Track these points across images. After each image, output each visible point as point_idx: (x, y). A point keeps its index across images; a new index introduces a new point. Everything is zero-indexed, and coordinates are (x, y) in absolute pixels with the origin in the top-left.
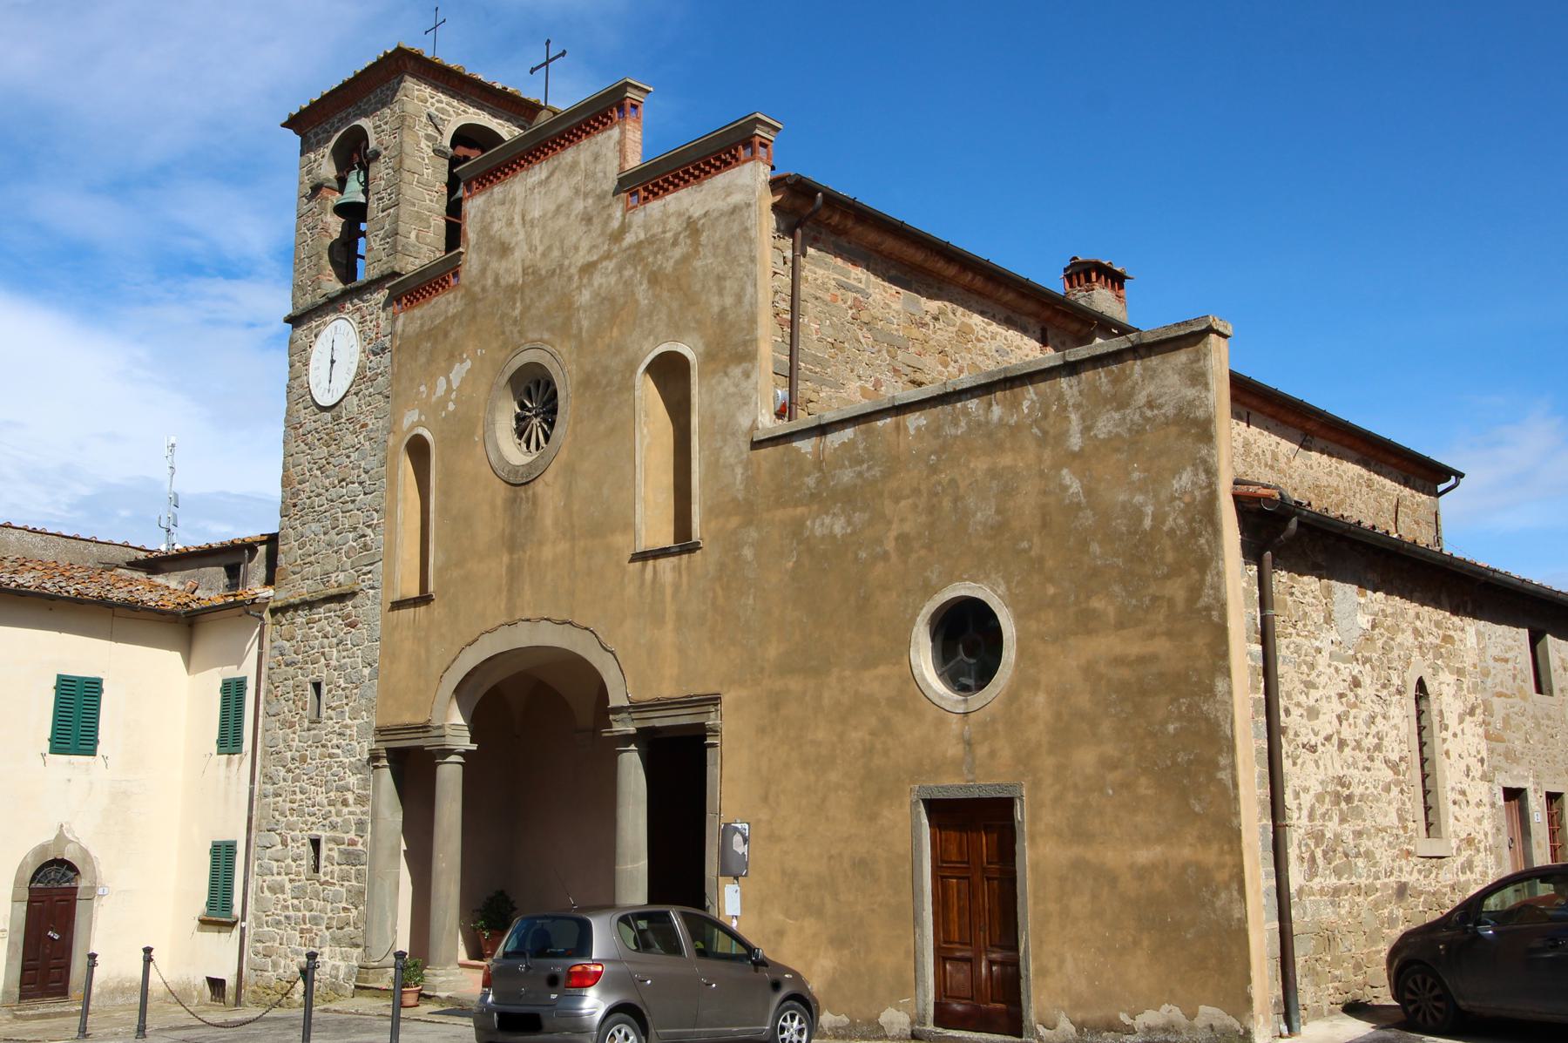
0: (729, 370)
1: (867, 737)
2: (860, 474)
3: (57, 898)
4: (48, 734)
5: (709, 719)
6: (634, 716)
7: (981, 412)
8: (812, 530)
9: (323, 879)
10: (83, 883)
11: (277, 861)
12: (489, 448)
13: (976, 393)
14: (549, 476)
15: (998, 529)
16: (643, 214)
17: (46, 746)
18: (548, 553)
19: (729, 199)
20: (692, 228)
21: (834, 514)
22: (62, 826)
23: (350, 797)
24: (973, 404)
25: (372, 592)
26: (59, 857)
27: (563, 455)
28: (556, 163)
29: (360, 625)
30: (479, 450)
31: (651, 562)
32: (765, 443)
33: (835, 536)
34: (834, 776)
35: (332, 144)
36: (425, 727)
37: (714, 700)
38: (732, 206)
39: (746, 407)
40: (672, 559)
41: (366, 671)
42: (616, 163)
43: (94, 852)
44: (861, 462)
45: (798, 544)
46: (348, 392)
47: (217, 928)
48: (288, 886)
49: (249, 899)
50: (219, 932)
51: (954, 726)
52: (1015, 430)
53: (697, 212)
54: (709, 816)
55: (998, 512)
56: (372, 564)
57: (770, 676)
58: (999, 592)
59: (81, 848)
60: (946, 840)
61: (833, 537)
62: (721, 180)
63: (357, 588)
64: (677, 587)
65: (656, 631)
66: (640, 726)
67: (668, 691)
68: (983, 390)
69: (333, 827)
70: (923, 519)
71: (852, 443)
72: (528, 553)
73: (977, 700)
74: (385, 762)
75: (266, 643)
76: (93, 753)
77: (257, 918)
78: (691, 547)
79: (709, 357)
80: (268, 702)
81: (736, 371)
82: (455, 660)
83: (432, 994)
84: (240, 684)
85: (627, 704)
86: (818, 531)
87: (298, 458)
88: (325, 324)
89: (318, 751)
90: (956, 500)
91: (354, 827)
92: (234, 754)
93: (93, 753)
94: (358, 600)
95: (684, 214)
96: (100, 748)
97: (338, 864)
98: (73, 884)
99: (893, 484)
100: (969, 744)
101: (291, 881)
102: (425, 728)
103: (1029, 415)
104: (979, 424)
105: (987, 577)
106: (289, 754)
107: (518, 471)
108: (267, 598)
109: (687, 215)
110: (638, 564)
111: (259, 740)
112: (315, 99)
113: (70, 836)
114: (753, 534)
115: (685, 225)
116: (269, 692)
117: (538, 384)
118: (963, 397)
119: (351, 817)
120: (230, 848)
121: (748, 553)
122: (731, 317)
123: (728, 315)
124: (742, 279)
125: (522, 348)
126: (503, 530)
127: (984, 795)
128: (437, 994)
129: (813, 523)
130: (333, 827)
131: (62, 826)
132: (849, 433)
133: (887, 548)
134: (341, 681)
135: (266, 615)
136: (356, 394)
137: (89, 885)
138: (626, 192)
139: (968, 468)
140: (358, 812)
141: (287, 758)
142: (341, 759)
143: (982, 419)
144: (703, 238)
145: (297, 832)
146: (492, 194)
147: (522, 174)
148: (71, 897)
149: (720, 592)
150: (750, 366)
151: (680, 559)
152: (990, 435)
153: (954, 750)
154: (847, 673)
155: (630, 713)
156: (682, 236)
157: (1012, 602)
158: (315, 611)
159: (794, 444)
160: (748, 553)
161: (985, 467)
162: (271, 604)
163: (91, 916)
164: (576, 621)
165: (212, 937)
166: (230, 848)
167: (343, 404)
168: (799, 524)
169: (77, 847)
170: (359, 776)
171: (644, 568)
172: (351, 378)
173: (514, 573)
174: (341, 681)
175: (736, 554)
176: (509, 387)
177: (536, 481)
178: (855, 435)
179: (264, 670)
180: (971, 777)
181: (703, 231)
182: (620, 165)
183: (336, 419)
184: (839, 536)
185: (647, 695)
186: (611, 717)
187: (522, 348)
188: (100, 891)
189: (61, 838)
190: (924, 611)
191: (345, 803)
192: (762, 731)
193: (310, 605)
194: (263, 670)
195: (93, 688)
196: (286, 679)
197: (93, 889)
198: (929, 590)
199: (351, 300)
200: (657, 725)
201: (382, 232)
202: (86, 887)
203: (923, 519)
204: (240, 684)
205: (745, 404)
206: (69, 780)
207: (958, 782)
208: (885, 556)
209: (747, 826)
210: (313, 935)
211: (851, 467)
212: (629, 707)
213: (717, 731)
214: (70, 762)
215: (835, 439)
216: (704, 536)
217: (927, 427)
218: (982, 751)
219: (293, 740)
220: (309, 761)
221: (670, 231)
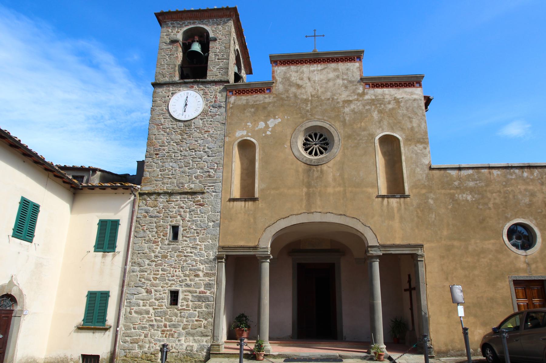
0: (417, 145)
1: (489, 261)
2: (476, 184)
3: (3, 315)
4: (13, 226)
6: (381, 249)
7: (520, 173)
8: (458, 197)
9: (180, 308)
10: (17, 308)
12: (294, 150)
13: (517, 168)
14: (330, 164)
15: (530, 205)
17: (11, 232)
18: (330, 190)
20: (397, 101)
21: (467, 194)
22: (12, 277)
23: (201, 273)
24: (517, 171)
26: (9, 293)
27: (338, 158)
28: (326, 66)
29: (206, 206)
30: (288, 151)
32: (435, 169)
33: (468, 200)
34: (476, 272)
35: (185, 28)
36: (255, 247)
37: (421, 246)
38: (414, 98)
40: (396, 199)
41: (211, 224)
42: (359, 73)
43: (25, 292)
44: (477, 181)
46: (196, 117)
47: (92, 331)
48: (152, 311)
49: (121, 318)
50: (93, 333)
51: (522, 259)
52: (532, 180)
53: (399, 96)
54: (421, 284)
55: (530, 201)
56: (215, 183)
57: (445, 240)
58: (533, 222)
59: (19, 289)
60: (518, 292)
61: (467, 201)
62: (409, 90)
64: (399, 210)
65: (390, 222)
66: (384, 252)
67: (398, 242)
68: (521, 167)
69: (187, 285)
70: (503, 199)
71: (473, 175)
72: (319, 189)
73: (529, 252)
74: (224, 260)
75: (136, 207)
76: (31, 241)
77: (125, 326)
79: (408, 140)
80: (136, 232)
81: (421, 146)
82: (354, 218)
83: (268, 354)
84: (115, 224)
85: (378, 245)
86: (461, 198)
88: (180, 90)
89: (176, 254)
90: (514, 196)
91: (203, 286)
92: (108, 252)
93: (31, 241)
94: (205, 196)
95: (392, 96)
96: (35, 239)
97: (191, 301)
98: (12, 308)
99: (490, 188)
100: (528, 264)
101: (154, 309)
102: (255, 248)
103: (536, 177)
104: (520, 177)
105: (528, 218)
106: (153, 254)
107: (312, 161)
108: (139, 188)
109: (394, 96)
110: (380, 199)
111: (130, 246)
113: (15, 282)
114: (432, 195)
117: (316, 135)
118: (513, 168)
119: (202, 282)
120: (105, 295)
122: (416, 130)
124: (419, 120)
126: (303, 180)
127: (536, 279)
128: (271, 353)
129: (459, 195)
130: (187, 285)
131: (12, 277)
132: (470, 172)
133: (490, 206)
134: (194, 227)
135: (137, 194)
136: (201, 119)
137: (20, 309)
138: (364, 83)
139: (518, 188)
141: (152, 256)
143: (521, 175)
144: (402, 104)
145: (160, 288)
146: (290, 68)
148: (10, 315)
149: (420, 212)
150: (426, 146)
152: (524, 180)
153: (523, 266)
154: (478, 241)
155: (379, 248)
157: (538, 225)
158: (172, 197)
159: (448, 171)
161: (523, 188)
163: (19, 326)
164: (348, 215)
166: (105, 295)
167: (193, 121)
168: (453, 195)
169: (18, 288)
170: (206, 265)
172: (199, 113)
173: (309, 196)
174: (194, 227)
175: (426, 201)
176: (303, 132)
177: (323, 165)
178: (473, 173)
179: (135, 218)
180: (530, 274)
183: (189, 126)
184: (470, 200)
185: (388, 243)
186: (369, 249)
188: (25, 313)
189: (11, 283)
190: (507, 225)
191: (197, 276)
192: (442, 257)
193: (171, 194)
194: (134, 218)
195: (36, 208)
196: (150, 223)
197: (22, 311)
198: (507, 220)
200: (393, 253)
201: (218, 66)
202: (19, 310)
203: (503, 199)
204: (115, 224)
205: (425, 156)
206: (19, 253)
207: (526, 275)
208: (490, 209)
210: (172, 332)
211: (472, 181)
212: (379, 246)
213: (423, 256)
214: (20, 243)
215: (464, 173)
217: (501, 175)
218: (533, 266)
219: (156, 248)
220: (169, 257)
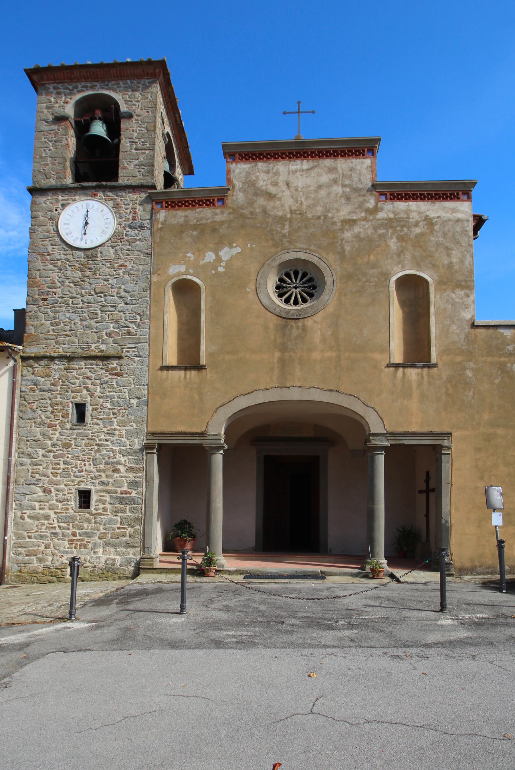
0: (455, 291)
5: (444, 442)
6: (389, 438)
11: (40, 502)
14: (318, 317)
16: (391, 206)
18: (316, 355)
19: (454, 215)
20: (429, 222)
25: (137, 359)
27: (330, 309)
28: (316, 164)
30: (252, 296)
31: (401, 370)
37: (449, 435)
39: (468, 310)
40: (416, 370)
42: (369, 176)
45: (501, 373)
49: (9, 524)
56: (138, 343)
62: (449, 204)
63: (123, 355)
66: (393, 442)
67: (414, 429)
72: (299, 354)
74: (155, 451)
78: (431, 366)
79: (441, 283)
81: (462, 293)
83: (222, 569)
87: (49, 273)
88: (75, 200)
94: (124, 361)
102: (202, 435)
107: (289, 312)
108: (20, 350)
110: (392, 369)
112: (41, 66)
114: (472, 365)
115: (423, 219)
116: (20, 405)
121: (469, 373)
123: (454, 266)
125: (292, 250)
135: (17, 357)
138: (378, 192)
140: (131, 476)
141: (48, 445)
142: (110, 447)
146: (256, 165)
147: (286, 162)
150: (469, 292)
151: (423, 370)
156: (421, 223)
158: (72, 363)
159: (499, 330)
160: (469, 373)
162: (21, 354)
165: (503, 539)
171: (395, 374)
173: (283, 363)
179: (17, 392)
181: (436, 225)
182: (372, 178)
186: (371, 438)
187: (292, 250)
192: (478, 450)
199: (104, 192)
205: (467, 308)
209: (501, 488)
212: (386, 434)
216: (440, 362)
221: (412, 218)
